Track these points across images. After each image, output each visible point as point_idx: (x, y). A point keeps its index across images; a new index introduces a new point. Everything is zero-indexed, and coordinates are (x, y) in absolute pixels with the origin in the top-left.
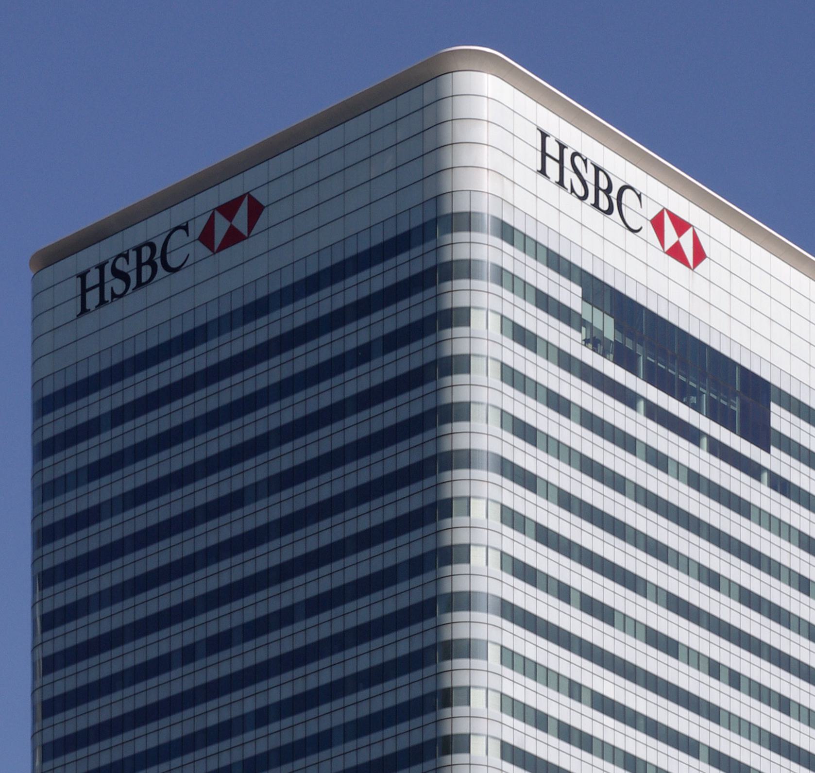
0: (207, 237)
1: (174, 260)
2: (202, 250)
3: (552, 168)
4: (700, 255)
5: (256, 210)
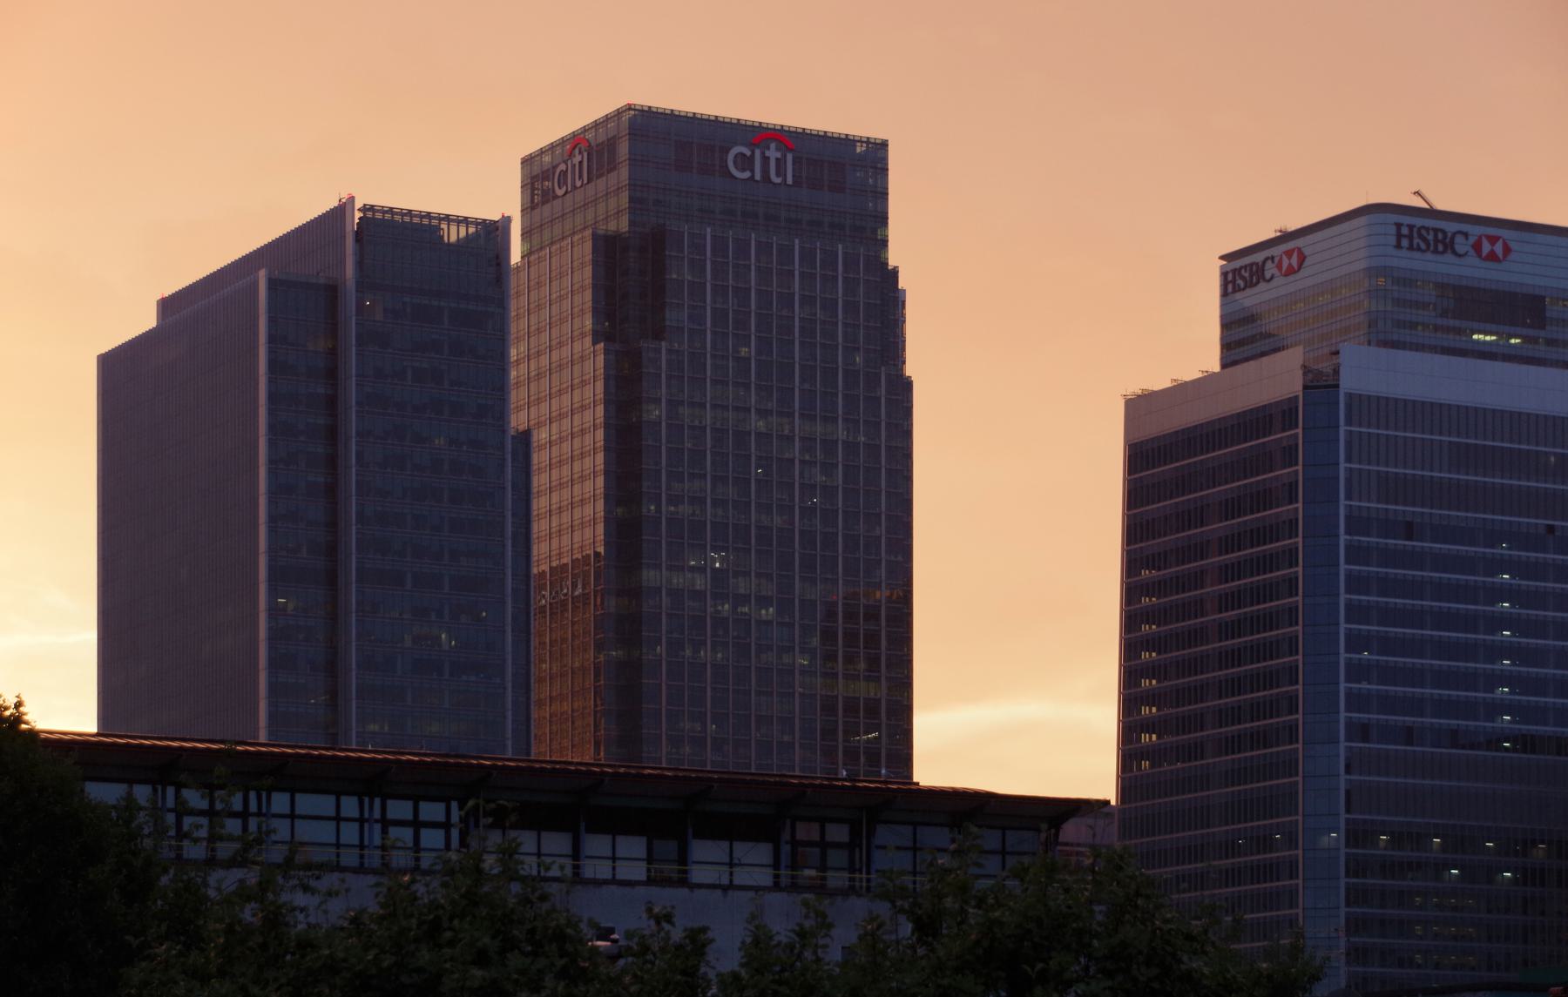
0: (1279, 267)
1: (1268, 276)
2: (1275, 271)
3: (1405, 243)
4: (1507, 250)
5: (1302, 258)
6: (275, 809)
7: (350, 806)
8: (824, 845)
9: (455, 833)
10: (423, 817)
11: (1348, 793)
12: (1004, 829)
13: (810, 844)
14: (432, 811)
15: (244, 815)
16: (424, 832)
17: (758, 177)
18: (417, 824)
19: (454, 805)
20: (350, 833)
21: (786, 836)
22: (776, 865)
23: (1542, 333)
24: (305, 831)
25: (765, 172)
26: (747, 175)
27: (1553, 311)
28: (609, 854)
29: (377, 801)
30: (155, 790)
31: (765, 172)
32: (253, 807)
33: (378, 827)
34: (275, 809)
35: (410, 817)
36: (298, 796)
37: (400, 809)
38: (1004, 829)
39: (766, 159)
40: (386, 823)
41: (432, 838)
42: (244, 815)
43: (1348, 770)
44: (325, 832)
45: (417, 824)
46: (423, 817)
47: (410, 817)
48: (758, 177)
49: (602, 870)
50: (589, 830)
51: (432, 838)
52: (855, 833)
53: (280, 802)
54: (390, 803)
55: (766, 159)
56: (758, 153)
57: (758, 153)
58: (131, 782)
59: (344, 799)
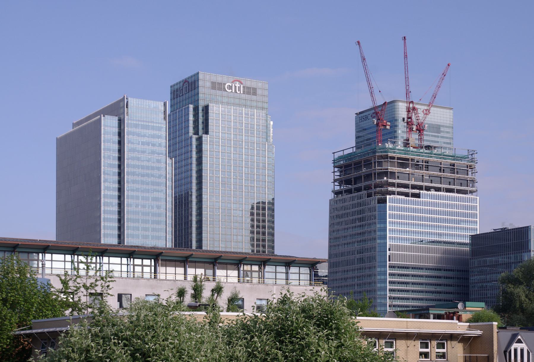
0: (372, 116)
6: (104, 262)
7: (124, 260)
8: (251, 271)
9: (153, 268)
10: (144, 264)
11: (389, 256)
12: (276, 266)
13: (249, 271)
14: (147, 262)
15: (96, 263)
16: (144, 268)
17: (233, 91)
18: (142, 266)
19: (153, 260)
20: (124, 268)
21: (242, 269)
22: (239, 277)
23: (440, 135)
24: (55, 265)
25: (235, 90)
26: (231, 91)
27: (442, 129)
28: (298, 279)
29: (132, 259)
30: (128, 260)
31: (235, 90)
32: (98, 261)
33: (132, 267)
34: (104, 262)
35: (141, 264)
36: (53, 255)
37: (138, 261)
38: (276, 266)
39: (235, 87)
40: (134, 265)
41: (147, 269)
42: (96, 263)
43: (389, 250)
44: (61, 265)
45: (142, 266)
46: (144, 264)
47: (141, 264)
48: (233, 91)
49: (162, 277)
50: (218, 269)
51: (147, 269)
52: (260, 268)
53: (106, 259)
54: (135, 260)
55: (235, 87)
56: (233, 85)
57: (233, 85)
58: (251, 265)
59: (66, 256)
